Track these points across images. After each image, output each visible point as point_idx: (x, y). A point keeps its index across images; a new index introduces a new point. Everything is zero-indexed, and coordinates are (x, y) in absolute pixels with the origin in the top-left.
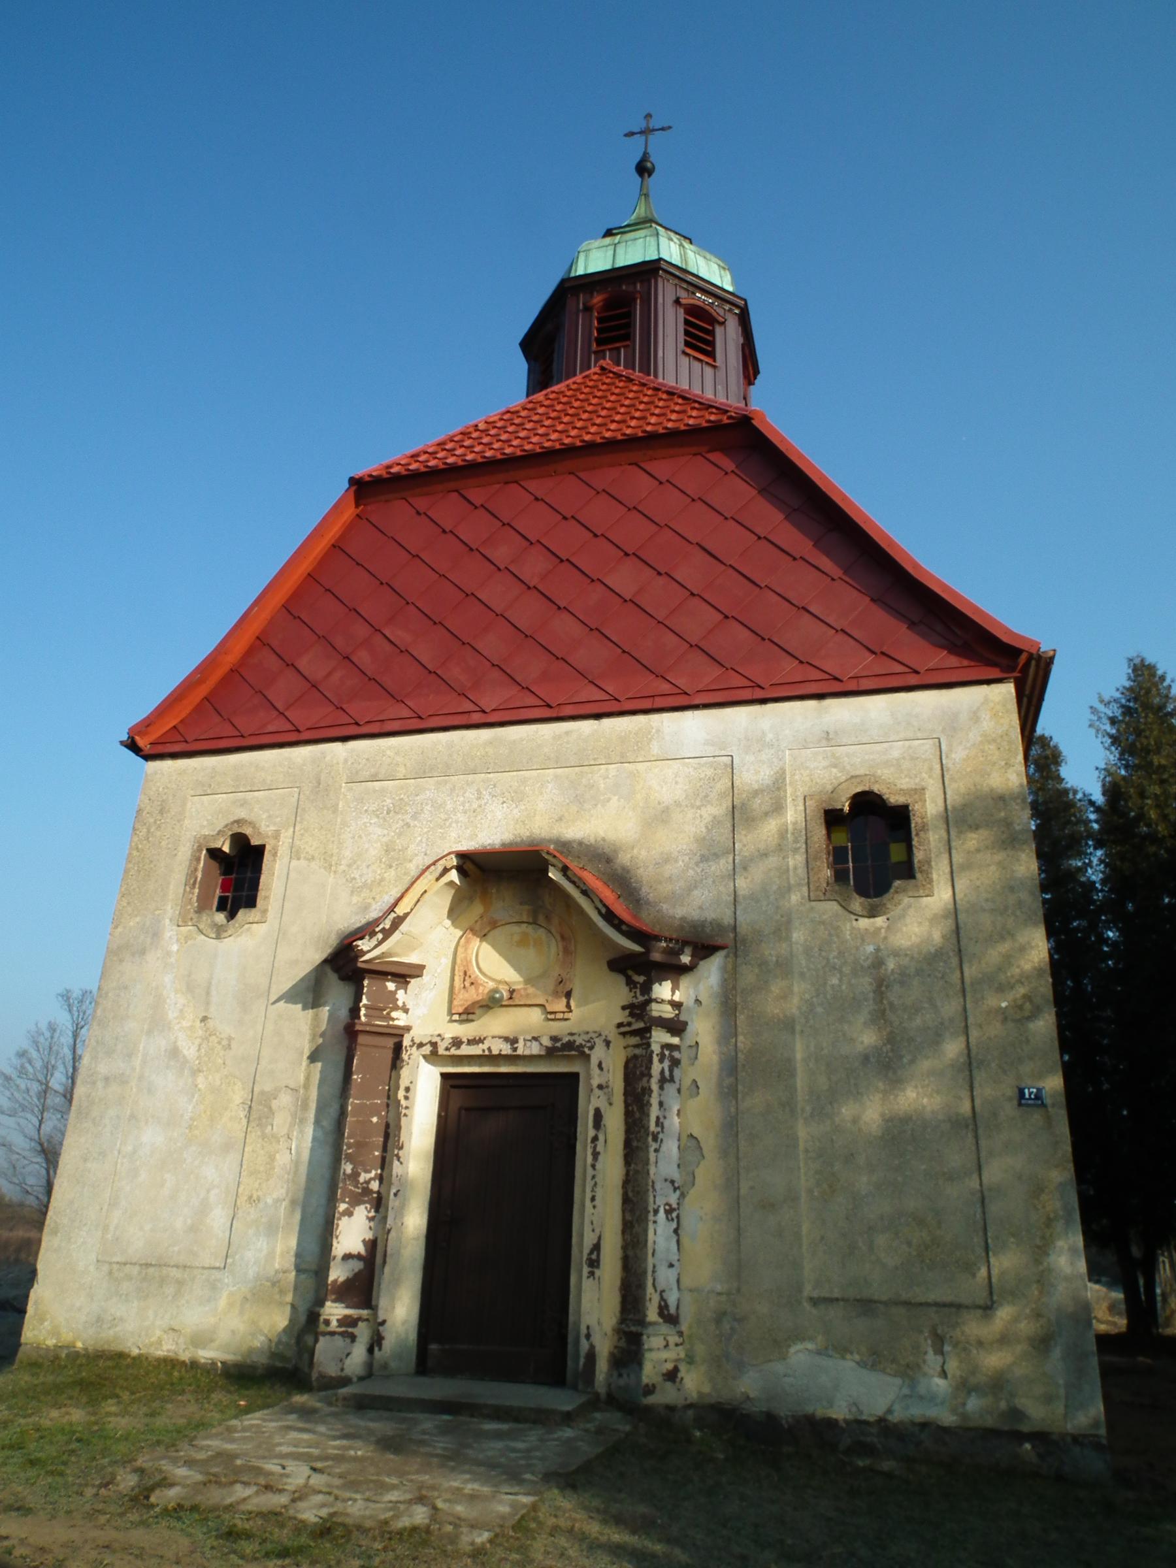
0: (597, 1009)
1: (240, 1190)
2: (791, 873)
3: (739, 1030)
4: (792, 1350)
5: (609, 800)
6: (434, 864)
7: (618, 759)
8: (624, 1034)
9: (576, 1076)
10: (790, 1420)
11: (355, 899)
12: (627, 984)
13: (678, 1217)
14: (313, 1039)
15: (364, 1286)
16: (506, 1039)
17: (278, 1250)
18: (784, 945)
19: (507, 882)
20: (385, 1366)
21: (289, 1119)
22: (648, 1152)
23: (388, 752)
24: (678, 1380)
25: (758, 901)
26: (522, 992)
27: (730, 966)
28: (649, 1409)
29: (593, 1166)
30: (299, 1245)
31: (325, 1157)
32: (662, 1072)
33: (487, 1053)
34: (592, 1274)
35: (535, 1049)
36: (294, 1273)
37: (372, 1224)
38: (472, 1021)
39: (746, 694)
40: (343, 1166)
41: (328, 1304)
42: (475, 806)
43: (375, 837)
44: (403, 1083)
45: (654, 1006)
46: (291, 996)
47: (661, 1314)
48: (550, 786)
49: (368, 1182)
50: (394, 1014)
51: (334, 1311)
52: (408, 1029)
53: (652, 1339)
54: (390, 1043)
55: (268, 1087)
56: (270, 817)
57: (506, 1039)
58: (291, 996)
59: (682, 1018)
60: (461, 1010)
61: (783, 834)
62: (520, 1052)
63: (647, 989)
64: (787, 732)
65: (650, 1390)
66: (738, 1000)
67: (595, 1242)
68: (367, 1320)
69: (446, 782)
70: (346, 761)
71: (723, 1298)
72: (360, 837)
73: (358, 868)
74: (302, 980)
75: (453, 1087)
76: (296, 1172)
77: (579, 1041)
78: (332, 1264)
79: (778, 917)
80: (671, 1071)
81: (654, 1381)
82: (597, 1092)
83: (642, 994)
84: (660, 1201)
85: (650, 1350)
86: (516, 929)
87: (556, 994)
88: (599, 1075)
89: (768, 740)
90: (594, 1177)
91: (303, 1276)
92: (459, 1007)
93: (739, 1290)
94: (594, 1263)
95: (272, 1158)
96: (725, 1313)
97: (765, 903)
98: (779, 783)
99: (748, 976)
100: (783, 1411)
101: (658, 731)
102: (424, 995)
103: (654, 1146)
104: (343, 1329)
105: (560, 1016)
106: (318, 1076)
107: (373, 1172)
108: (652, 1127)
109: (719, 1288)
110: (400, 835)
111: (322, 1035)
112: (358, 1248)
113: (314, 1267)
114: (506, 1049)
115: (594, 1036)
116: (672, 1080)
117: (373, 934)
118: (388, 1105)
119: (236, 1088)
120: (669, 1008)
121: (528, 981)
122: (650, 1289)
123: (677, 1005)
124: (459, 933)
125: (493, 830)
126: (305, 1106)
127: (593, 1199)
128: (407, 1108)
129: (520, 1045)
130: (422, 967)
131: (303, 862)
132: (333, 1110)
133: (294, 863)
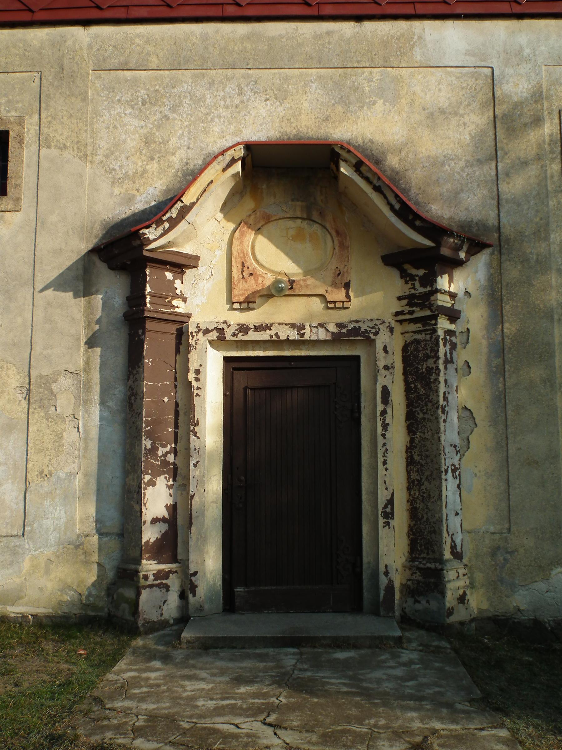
0: (375, 299)
1: (30, 466)
2: (549, 182)
3: (505, 318)
4: (554, 572)
5: (374, 103)
6: (222, 153)
7: (381, 63)
8: (401, 322)
9: (358, 358)
10: (551, 623)
11: (117, 191)
12: (402, 277)
13: (459, 475)
14: (89, 325)
15: (172, 544)
16: (293, 326)
17: (77, 518)
18: (544, 245)
19: (292, 178)
20: (201, 609)
21: (73, 400)
22: (438, 422)
23: (137, 41)
24: (466, 602)
25: (519, 205)
26: (302, 283)
27: (495, 263)
28: (450, 626)
29: (384, 436)
30: (97, 512)
31: (116, 434)
32: (446, 355)
33: (274, 338)
34: (387, 524)
35: (322, 335)
36: (96, 537)
37: (171, 491)
38: (254, 309)
39: (504, 8)
40: (144, 442)
41: (144, 562)
42: (237, 101)
43: (132, 128)
44: (193, 365)
45: (439, 296)
46: (60, 283)
47: (452, 553)
48: (314, 86)
49: (165, 455)
50: (175, 303)
51: (150, 566)
52: (189, 316)
53: (450, 573)
54: (173, 329)
55: (46, 372)
56: (9, 101)
57: (293, 326)
58: (60, 283)
59: (456, 307)
60: (241, 299)
61: (540, 146)
62: (306, 337)
63: (429, 280)
64: (543, 48)
65: (450, 612)
66: (504, 292)
67: (388, 498)
68: (176, 572)
69: (204, 76)
70: (90, 46)
71: (497, 536)
72: (115, 127)
73: (116, 159)
74: (68, 269)
75: (234, 369)
76: (86, 449)
77: (364, 327)
78: (143, 528)
79: (538, 219)
80: (451, 353)
81: (453, 605)
82: (383, 372)
83: (423, 285)
84: (449, 462)
85: (449, 581)
86: (290, 223)
87: (335, 285)
88: (385, 358)
89: (525, 54)
90: (384, 445)
91: (105, 539)
92: (239, 294)
93: (509, 530)
94: (389, 516)
95: (60, 437)
96: (498, 548)
97: (526, 207)
98: (538, 96)
99: (513, 272)
100: (546, 617)
101: (420, 38)
102: (201, 285)
103: (443, 417)
104: (159, 581)
105: (339, 305)
106: (98, 360)
107: (169, 446)
108: (442, 402)
109: (492, 529)
110: (159, 127)
111: (98, 322)
112: (162, 512)
113: (116, 530)
114: (294, 335)
115: (378, 323)
116: (452, 362)
117: (159, 222)
118: (176, 386)
119: (10, 372)
120: (448, 298)
121: (306, 273)
122: (445, 534)
123: (453, 296)
124: (231, 226)
125: (265, 123)
126: (88, 388)
127: (385, 463)
128: (198, 388)
129: (307, 330)
130: (197, 258)
131: (54, 152)
132: (119, 391)
133: (44, 151)
